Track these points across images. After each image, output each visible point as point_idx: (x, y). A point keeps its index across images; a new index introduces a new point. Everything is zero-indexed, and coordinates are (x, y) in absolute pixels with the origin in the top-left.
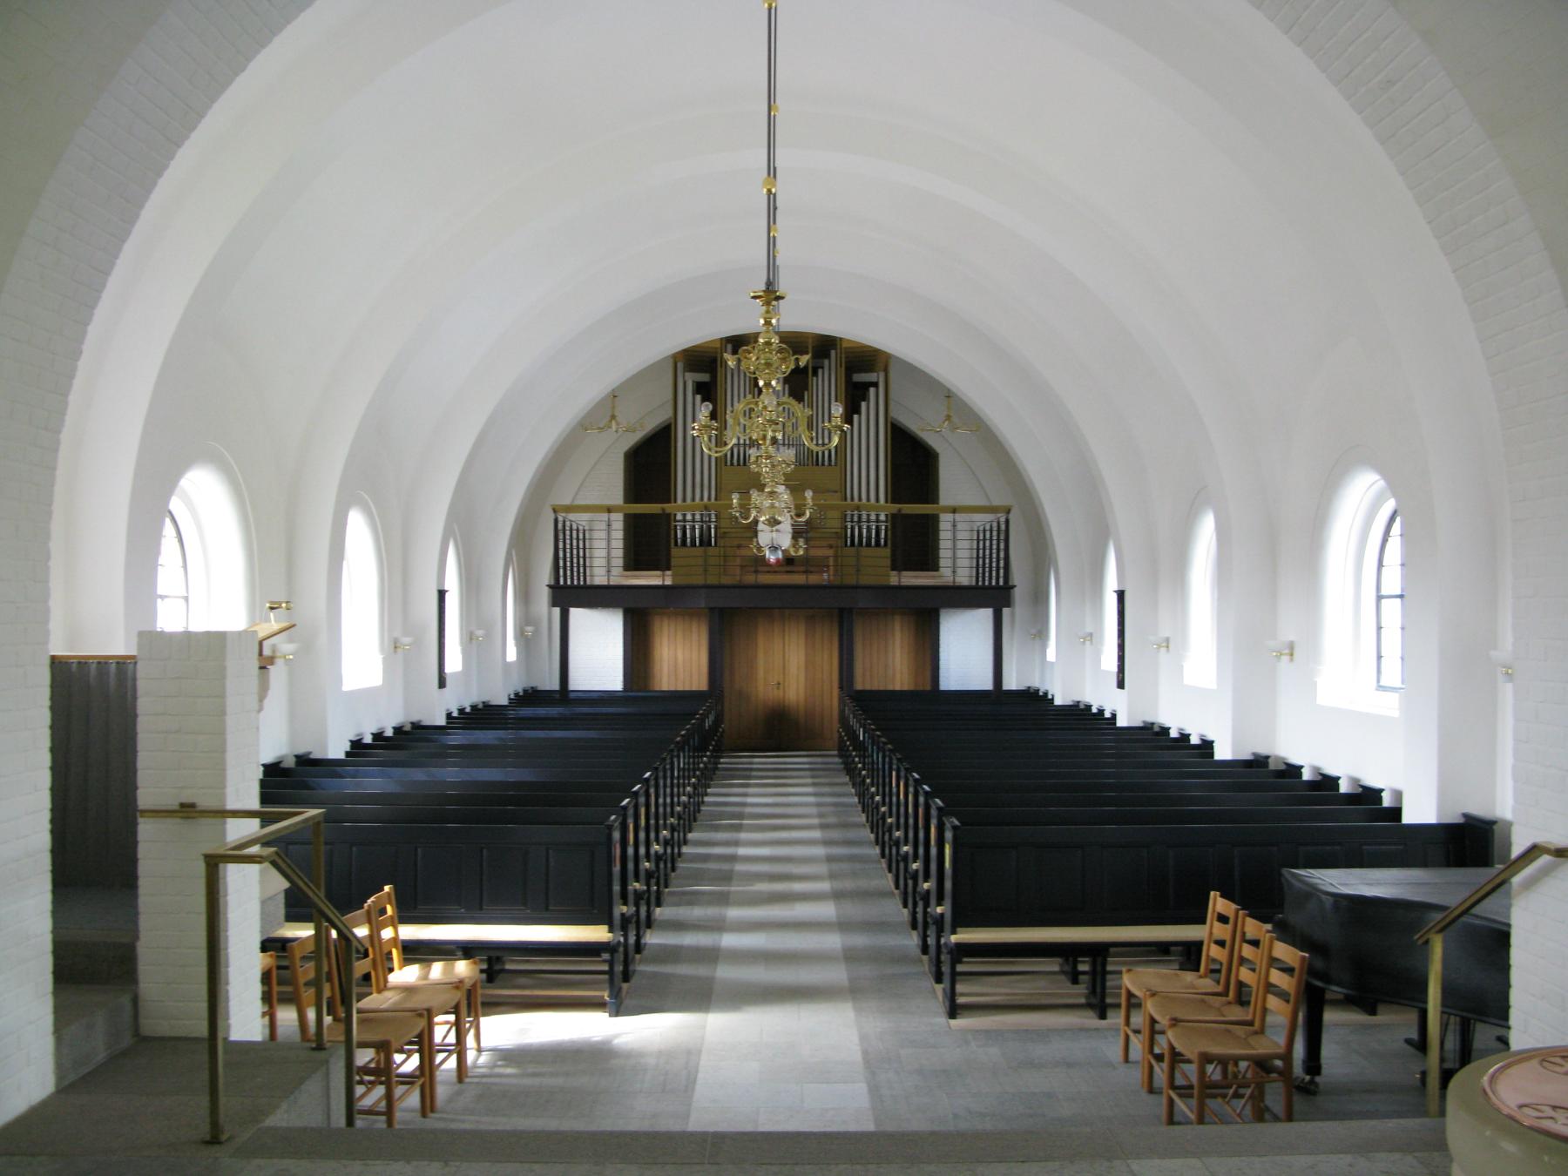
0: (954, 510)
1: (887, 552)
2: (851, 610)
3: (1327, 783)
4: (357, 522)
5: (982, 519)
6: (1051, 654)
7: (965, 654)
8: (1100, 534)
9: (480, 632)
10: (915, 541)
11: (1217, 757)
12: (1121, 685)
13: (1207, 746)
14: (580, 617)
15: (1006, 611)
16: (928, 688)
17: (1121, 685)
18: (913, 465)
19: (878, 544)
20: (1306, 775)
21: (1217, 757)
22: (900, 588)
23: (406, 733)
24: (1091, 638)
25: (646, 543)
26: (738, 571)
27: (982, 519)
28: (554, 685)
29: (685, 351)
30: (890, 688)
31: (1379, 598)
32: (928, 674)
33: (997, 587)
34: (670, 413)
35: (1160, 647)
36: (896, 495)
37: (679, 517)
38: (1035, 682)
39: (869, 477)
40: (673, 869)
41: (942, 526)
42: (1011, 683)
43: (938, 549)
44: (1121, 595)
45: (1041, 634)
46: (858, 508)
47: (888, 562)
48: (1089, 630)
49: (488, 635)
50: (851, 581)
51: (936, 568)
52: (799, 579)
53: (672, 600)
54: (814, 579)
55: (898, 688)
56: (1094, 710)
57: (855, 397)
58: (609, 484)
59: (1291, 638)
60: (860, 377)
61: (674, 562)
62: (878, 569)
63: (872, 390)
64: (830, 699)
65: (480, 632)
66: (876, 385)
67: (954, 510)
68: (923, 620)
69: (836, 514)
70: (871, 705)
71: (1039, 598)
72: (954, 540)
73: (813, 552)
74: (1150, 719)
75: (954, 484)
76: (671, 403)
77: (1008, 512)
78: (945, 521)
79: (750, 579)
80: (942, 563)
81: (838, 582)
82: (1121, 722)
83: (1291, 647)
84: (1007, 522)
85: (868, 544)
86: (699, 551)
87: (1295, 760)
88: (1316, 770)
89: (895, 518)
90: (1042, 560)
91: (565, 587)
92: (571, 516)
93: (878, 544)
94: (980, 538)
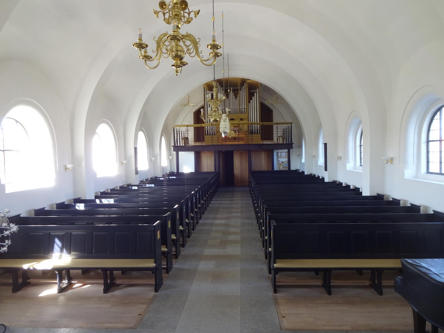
0: (277, 124)
1: (260, 135)
2: (250, 151)
3: (348, 186)
4: (141, 135)
5: (285, 126)
6: (303, 161)
7: (280, 160)
8: (319, 127)
9: (153, 159)
10: (267, 132)
11: (325, 181)
12: (326, 170)
13: (323, 179)
14: (182, 154)
15: (291, 150)
16: (271, 170)
17: (326, 170)
18: (266, 113)
19: (257, 133)
20: (344, 185)
21: (325, 181)
22: (263, 144)
23: (125, 188)
24: (315, 157)
25: (200, 134)
26: (221, 141)
27: (285, 126)
28: (175, 171)
29: (206, 84)
30: (261, 170)
31: (428, 141)
32: (271, 167)
33: (289, 144)
34: (203, 103)
35: (338, 159)
36: (262, 120)
37: (206, 128)
38: (298, 168)
39: (255, 116)
40: (208, 206)
41: (274, 128)
42: (293, 168)
43: (273, 134)
44: (325, 145)
45: (300, 156)
46: (252, 124)
47: (260, 138)
48: (314, 154)
49: (156, 159)
50: (250, 143)
51: (272, 139)
52: (236, 143)
53: (206, 148)
54: (241, 143)
55: (263, 170)
56: (316, 176)
57: (251, 96)
58: (190, 120)
59: (392, 156)
60: (252, 91)
61: (205, 139)
62: (257, 139)
63: (255, 94)
64: (246, 174)
65: (153, 159)
66: (256, 92)
67: (277, 124)
68: (269, 151)
69: (246, 125)
70: (254, 174)
71: (300, 146)
72: (277, 131)
73: (240, 136)
74: (335, 180)
75: (276, 118)
76: (203, 100)
77: (291, 123)
78: (275, 127)
79: (224, 143)
80: (274, 138)
81: (247, 143)
82: (326, 180)
83: (392, 159)
84: (291, 126)
85: (255, 133)
86: (211, 136)
87: (341, 182)
88: (346, 183)
89: (262, 126)
90: (301, 136)
91: (178, 146)
92: (181, 128)
93: (257, 133)
94: (284, 131)
